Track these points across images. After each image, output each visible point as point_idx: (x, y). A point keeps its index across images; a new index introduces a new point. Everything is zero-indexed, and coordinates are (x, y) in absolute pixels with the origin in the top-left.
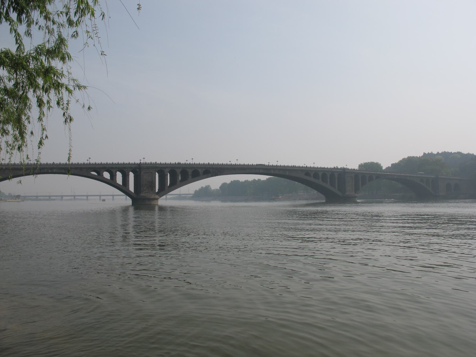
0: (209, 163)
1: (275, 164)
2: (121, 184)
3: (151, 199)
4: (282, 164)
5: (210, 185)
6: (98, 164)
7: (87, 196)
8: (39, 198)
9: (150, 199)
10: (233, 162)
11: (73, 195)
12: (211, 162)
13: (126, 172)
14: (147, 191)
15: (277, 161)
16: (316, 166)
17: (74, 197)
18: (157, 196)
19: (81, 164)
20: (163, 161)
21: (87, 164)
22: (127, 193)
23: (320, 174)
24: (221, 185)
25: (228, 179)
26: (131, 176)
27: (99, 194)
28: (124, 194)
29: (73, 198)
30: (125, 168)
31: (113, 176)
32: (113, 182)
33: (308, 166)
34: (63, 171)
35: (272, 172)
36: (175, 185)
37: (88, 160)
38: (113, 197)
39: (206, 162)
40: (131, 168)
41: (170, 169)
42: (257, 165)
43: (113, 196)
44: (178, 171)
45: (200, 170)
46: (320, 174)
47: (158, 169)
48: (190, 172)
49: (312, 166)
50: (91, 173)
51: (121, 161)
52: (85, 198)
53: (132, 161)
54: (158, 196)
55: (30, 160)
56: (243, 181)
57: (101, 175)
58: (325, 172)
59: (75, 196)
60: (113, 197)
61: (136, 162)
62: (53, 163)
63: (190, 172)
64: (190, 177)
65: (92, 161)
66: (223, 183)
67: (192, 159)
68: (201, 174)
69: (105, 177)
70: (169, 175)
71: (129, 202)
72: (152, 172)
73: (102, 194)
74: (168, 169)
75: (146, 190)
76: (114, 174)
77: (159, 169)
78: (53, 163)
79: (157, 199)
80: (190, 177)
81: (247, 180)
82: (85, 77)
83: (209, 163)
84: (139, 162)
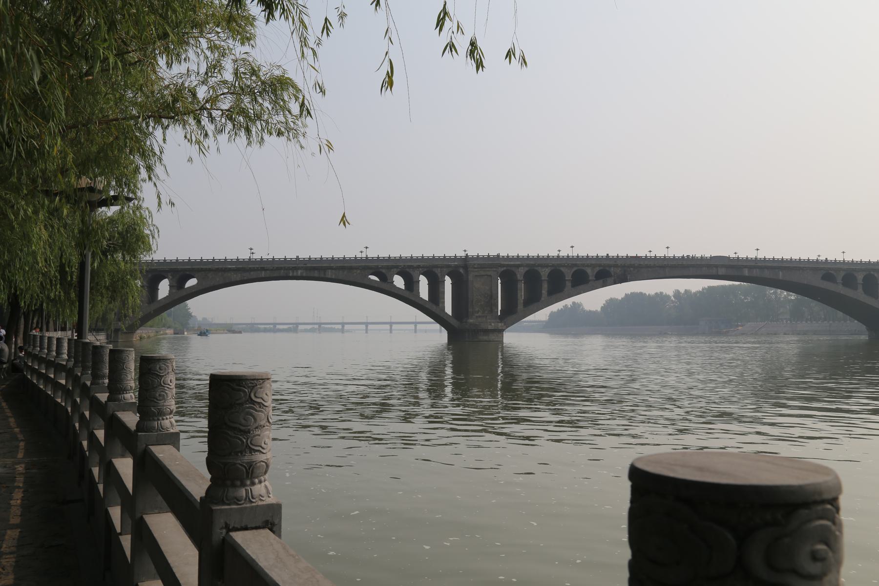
0: (608, 254)
1: (752, 255)
2: (427, 300)
3: (488, 330)
4: (769, 256)
5: (582, 303)
6: (183, 262)
7: (343, 324)
8: (278, 327)
9: (487, 332)
10: (660, 253)
11: (316, 322)
12: (613, 254)
13: (439, 275)
14: (480, 314)
15: (668, 248)
16: (848, 258)
17: (319, 326)
18: (500, 325)
19: (350, 260)
20: (513, 253)
21: (361, 259)
22: (439, 318)
23: (860, 277)
24: (604, 302)
25: (618, 291)
26: (448, 281)
27: (414, 321)
28: (432, 320)
29: (316, 326)
30: (437, 267)
31: (412, 284)
32: (409, 297)
33: (831, 258)
34: (238, 277)
35: (746, 272)
36: (534, 302)
37: (361, 252)
38: (367, 327)
39: (602, 253)
40: (448, 266)
41: (527, 269)
42: (711, 257)
43: (416, 323)
44: (520, 274)
45: (589, 271)
46: (860, 277)
47: (502, 269)
48: (568, 274)
49: (840, 258)
50: (370, 276)
51: (428, 253)
52: (340, 327)
53: (450, 253)
54: (503, 324)
55: (253, 253)
56: (652, 293)
57: (388, 281)
58: (872, 273)
59: (320, 324)
60: (367, 327)
61: (241, 257)
62: (298, 257)
63: (568, 274)
64: (569, 284)
65: (372, 254)
66: (608, 298)
67: (758, 250)
68: (590, 278)
69: (397, 286)
70: (499, 281)
71: (439, 336)
72: (490, 276)
73: (346, 321)
74: (522, 268)
75: (478, 312)
76: (415, 280)
77: (505, 268)
78: (298, 257)
79: (501, 331)
80: (569, 284)
81: (661, 293)
82: (305, 84)
83: (608, 254)
84: (463, 254)
